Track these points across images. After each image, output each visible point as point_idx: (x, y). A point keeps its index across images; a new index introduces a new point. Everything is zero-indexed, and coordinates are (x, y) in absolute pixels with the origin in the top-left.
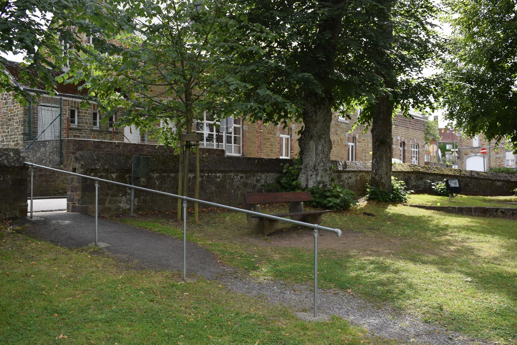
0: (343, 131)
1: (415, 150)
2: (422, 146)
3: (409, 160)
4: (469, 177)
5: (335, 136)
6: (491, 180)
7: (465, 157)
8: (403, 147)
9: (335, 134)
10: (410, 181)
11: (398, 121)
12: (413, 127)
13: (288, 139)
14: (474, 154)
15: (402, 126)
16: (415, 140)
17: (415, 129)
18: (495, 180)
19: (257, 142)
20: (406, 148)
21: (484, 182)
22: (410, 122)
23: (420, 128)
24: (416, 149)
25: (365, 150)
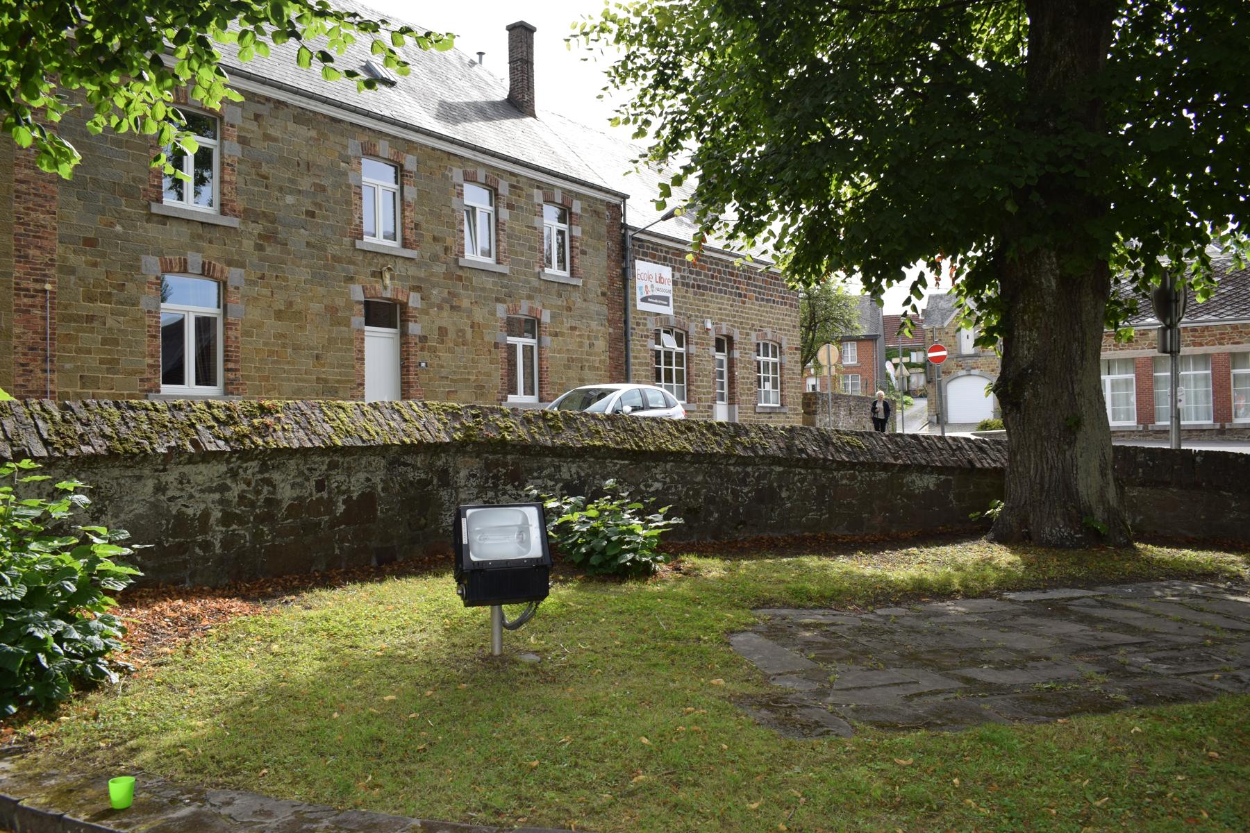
0: (485, 298)
1: (771, 359)
2: (790, 348)
3: (749, 389)
4: (775, 460)
5: (445, 314)
6: (886, 467)
7: (944, 378)
8: (402, 326)
9: (447, 307)
10: (444, 494)
11: (706, 275)
12: (759, 293)
13: (532, 347)
14: (964, 372)
15: (720, 291)
16: (768, 331)
17: (768, 301)
18: (905, 468)
19: (17, 331)
20: (737, 354)
21: (853, 478)
22: (750, 278)
23: (783, 298)
24: (774, 356)
25: (581, 360)
